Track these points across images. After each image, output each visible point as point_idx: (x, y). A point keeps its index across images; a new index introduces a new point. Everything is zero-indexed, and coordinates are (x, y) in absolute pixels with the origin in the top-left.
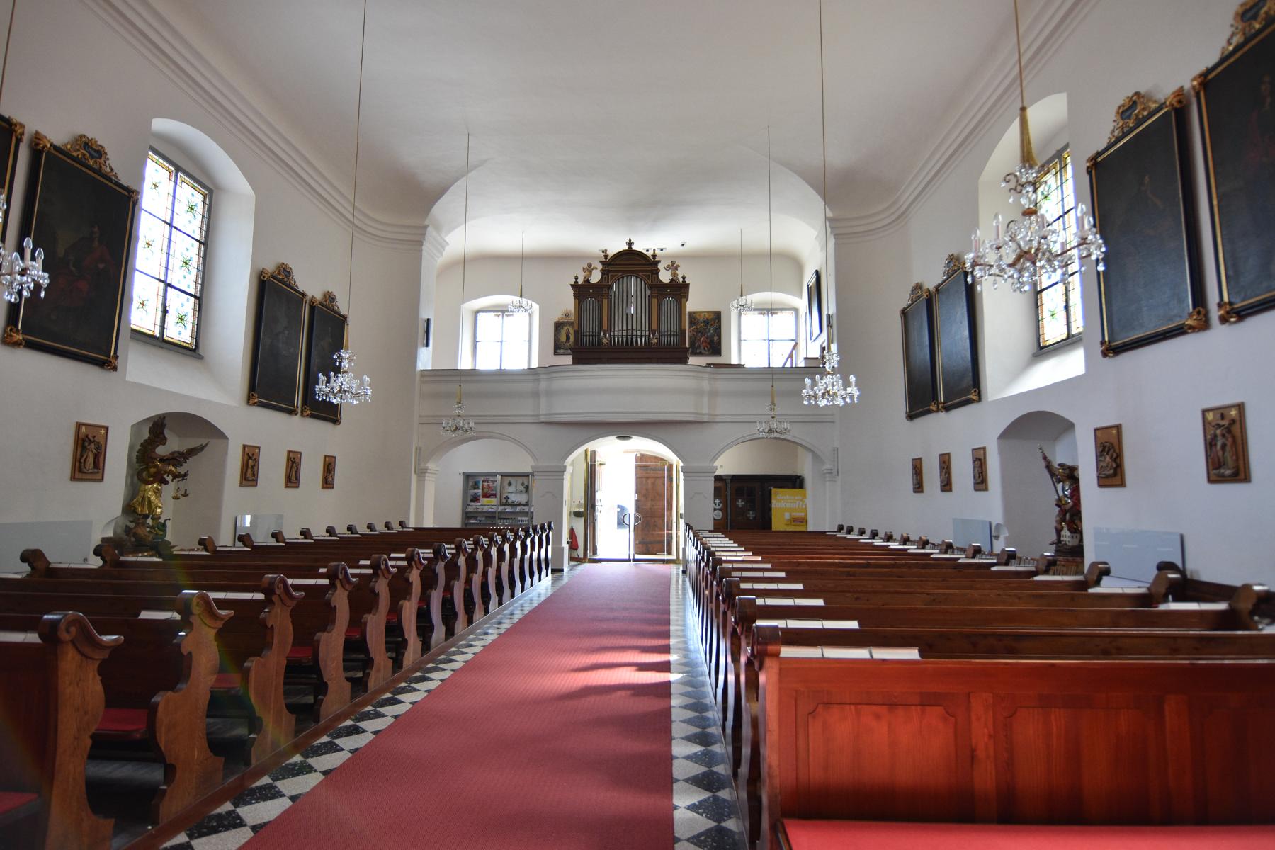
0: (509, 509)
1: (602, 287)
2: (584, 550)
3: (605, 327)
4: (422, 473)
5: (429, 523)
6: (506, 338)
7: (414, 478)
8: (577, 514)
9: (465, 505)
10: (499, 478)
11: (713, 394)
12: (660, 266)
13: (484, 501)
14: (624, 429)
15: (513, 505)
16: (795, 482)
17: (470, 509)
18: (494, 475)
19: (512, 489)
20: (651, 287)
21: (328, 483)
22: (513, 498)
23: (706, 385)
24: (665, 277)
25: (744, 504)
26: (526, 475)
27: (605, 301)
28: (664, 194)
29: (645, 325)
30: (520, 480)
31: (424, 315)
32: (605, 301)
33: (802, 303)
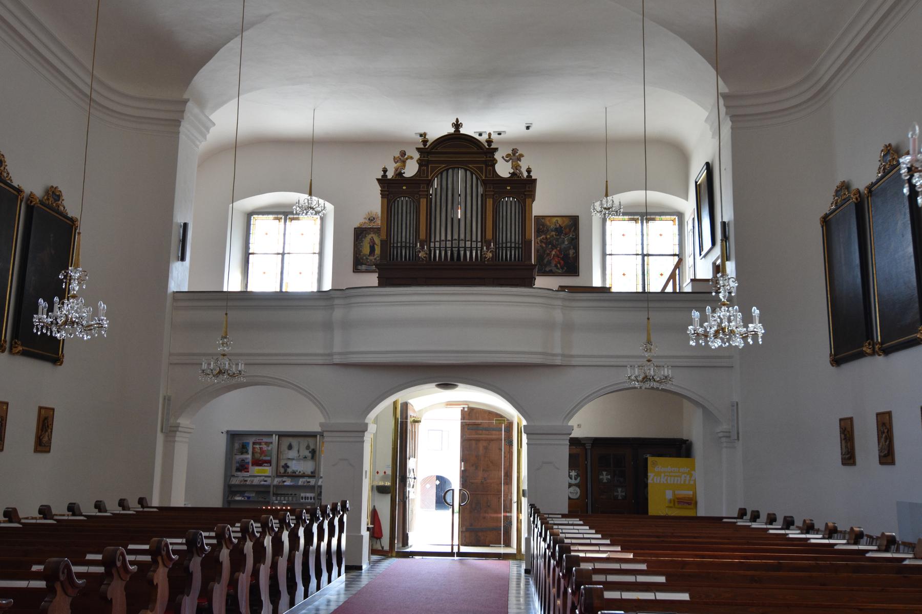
0: (288, 482)
1: (419, 184)
2: (391, 539)
3: (423, 235)
4: (171, 431)
5: (178, 500)
6: (289, 253)
7: (160, 438)
8: (381, 490)
9: (228, 476)
10: (275, 438)
11: (568, 327)
12: (497, 156)
13: (255, 470)
14: (446, 374)
15: (294, 476)
16: (679, 448)
17: (234, 481)
18: (269, 434)
19: (292, 454)
20: (485, 183)
21: (42, 444)
22: (295, 466)
23: (558, 315)
24: (503, 169)
25: (609, 479)
26: (313, 435)
27: (423, 202)
28: (496, 75)
29: (477, 234)
30: (304, 442)
31: (179, 219)
32: (423, 202)
33: (688, 206)
